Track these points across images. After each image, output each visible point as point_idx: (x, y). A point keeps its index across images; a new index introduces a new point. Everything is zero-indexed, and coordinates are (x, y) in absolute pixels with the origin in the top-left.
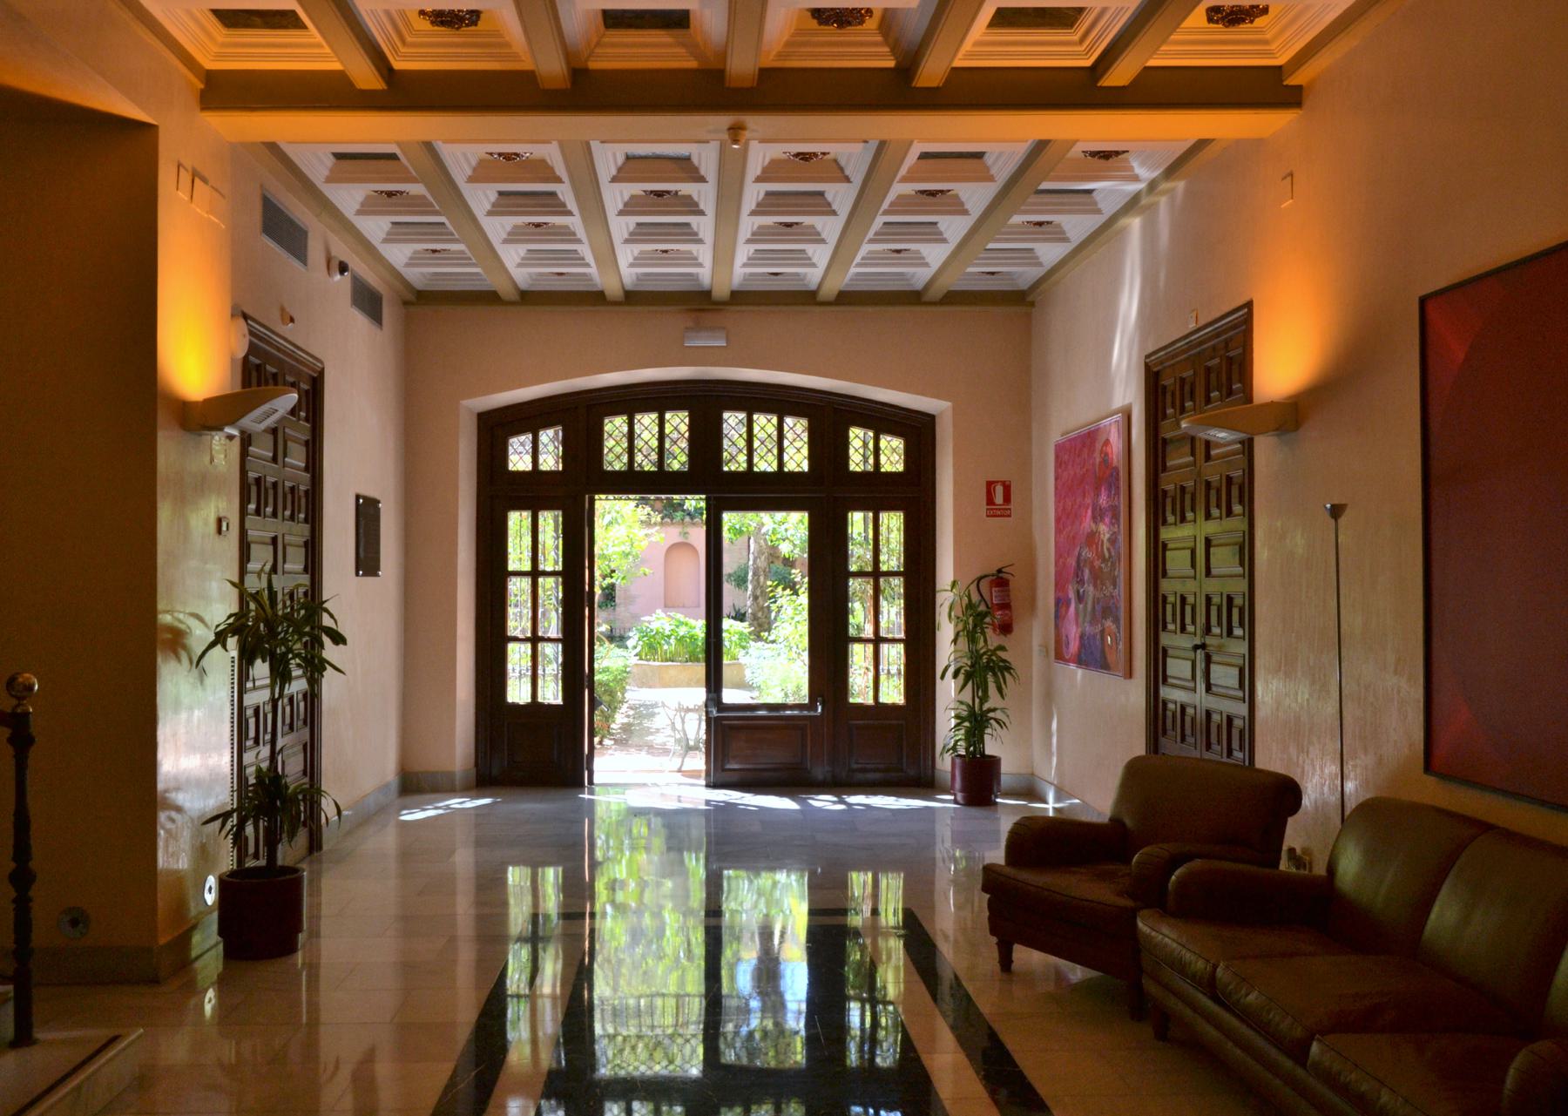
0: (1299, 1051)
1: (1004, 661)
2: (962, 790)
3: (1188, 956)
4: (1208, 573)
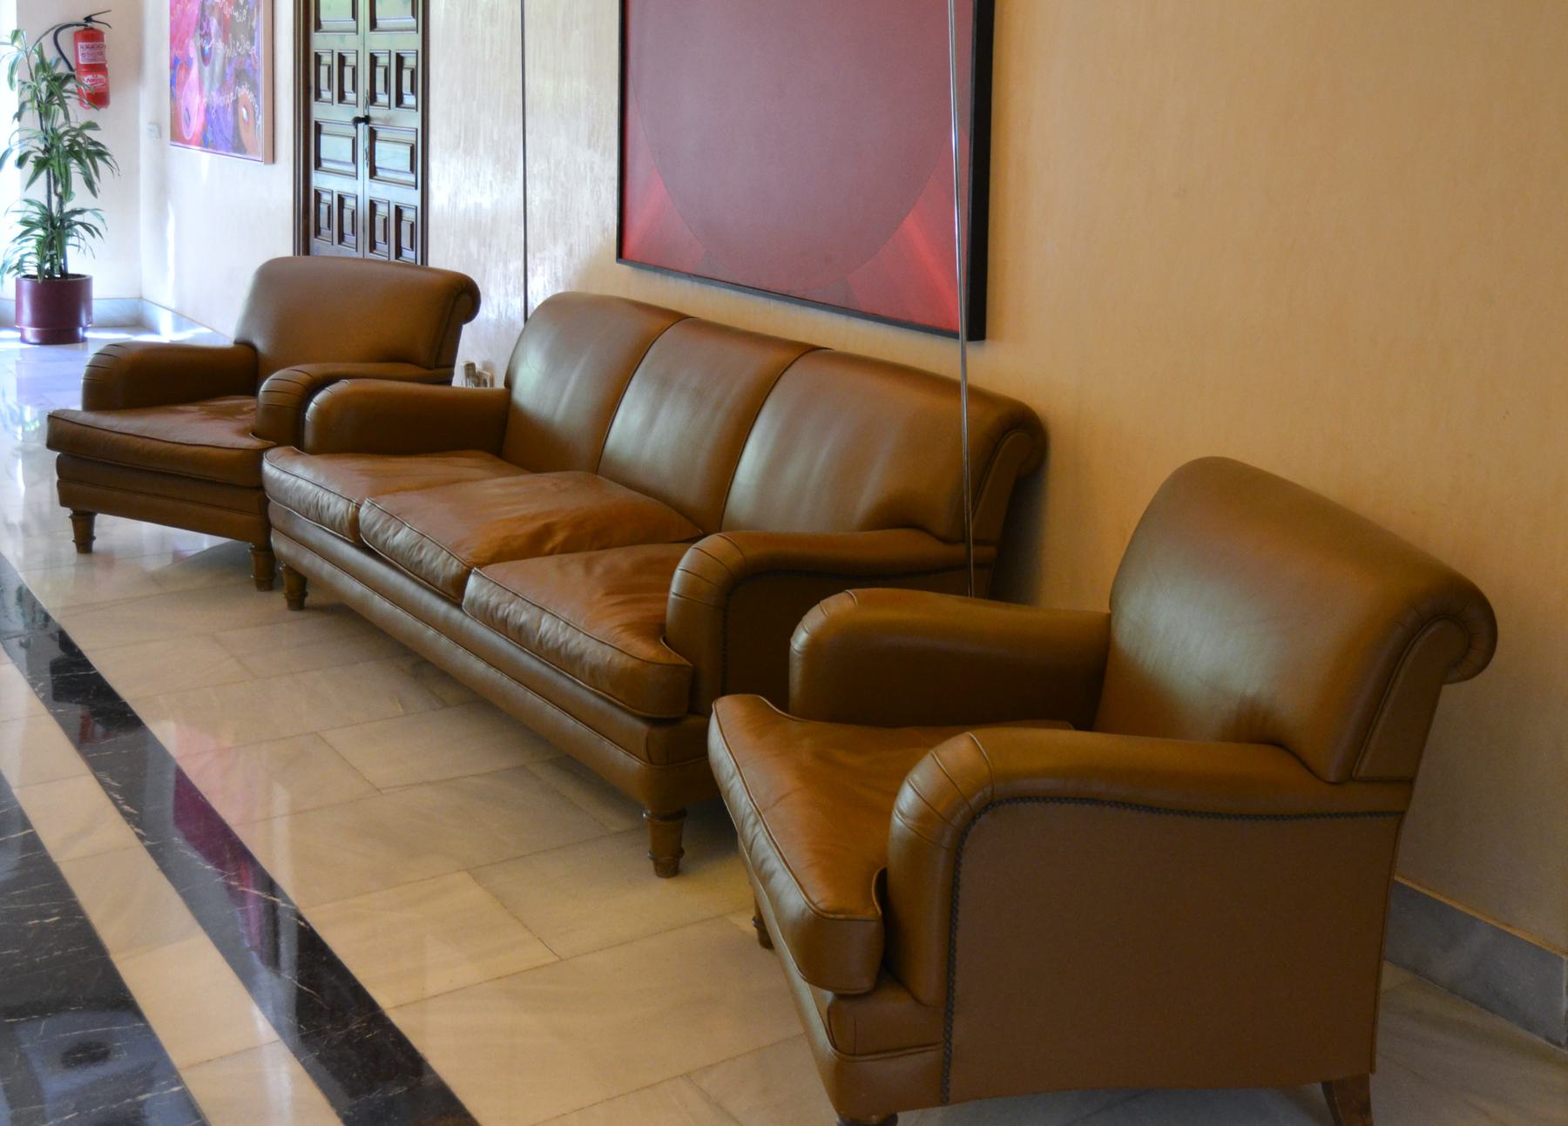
0: (453, 591)
1: (95, 144)
2: (36, 323)
3: (325, 498)
4: (373, 24)
